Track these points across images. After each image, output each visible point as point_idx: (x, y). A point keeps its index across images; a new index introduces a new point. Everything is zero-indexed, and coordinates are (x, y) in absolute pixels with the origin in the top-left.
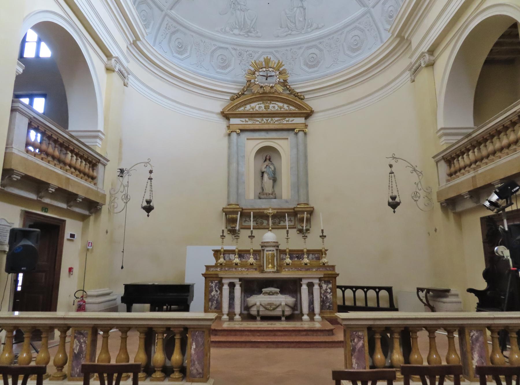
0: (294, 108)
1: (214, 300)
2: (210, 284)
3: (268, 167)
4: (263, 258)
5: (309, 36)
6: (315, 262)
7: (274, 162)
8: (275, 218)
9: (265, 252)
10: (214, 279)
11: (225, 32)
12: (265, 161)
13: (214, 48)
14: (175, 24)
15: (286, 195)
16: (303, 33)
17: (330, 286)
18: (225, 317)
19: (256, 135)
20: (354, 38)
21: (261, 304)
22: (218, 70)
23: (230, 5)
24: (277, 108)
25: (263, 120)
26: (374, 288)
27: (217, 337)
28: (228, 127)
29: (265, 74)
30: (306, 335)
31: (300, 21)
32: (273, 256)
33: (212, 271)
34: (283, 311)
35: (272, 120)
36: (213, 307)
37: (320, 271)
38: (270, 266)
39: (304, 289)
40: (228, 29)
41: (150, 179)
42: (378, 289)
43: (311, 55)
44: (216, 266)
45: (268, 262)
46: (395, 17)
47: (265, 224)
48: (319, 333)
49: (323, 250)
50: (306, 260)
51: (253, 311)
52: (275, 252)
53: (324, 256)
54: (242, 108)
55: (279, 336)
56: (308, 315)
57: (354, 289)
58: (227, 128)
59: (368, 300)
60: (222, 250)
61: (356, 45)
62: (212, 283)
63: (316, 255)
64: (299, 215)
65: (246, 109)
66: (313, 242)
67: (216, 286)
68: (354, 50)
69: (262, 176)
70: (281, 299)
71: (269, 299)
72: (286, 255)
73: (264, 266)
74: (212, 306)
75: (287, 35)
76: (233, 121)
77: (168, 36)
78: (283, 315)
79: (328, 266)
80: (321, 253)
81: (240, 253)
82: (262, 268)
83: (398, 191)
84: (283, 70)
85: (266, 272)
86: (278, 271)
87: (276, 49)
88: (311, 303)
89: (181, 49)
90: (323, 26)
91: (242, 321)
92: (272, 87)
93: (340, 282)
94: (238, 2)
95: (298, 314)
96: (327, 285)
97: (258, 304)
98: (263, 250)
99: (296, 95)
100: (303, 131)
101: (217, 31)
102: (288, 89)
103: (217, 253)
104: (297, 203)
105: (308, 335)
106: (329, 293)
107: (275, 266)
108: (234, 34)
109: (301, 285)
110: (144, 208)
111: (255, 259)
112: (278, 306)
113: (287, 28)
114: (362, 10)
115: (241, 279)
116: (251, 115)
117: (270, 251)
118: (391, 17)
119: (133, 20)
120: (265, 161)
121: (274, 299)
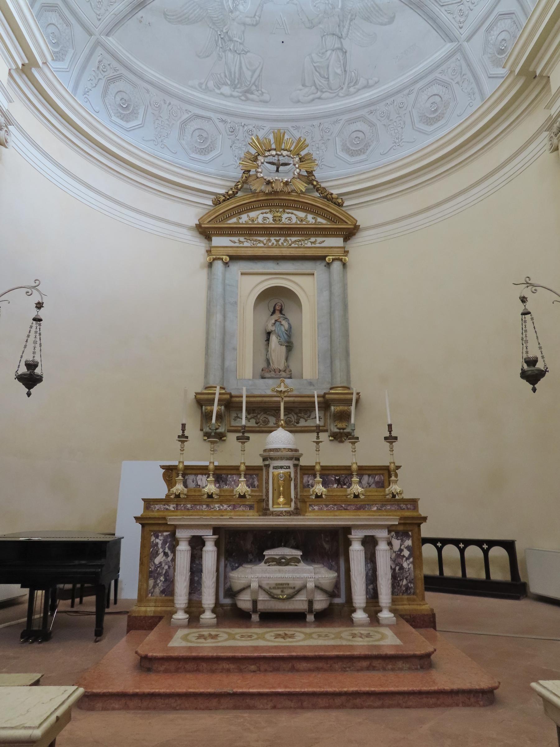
0: (324, 222)
1: (159, 574)
2: (153, 538)
3: (277, 323)
4: (267, 483)
5: (352, 100)
6: (375, 493)
7: (288, 316)
8: (289, 413)
9: (271, 470)
10: (162, 528)
11: (207, 90)
12: (274, 313)
13: (186, 116)
14: (115, 64)
15: (310, 373)
16: (341, 94)
17: (409, 542)
18: (181, 616)
19: (258, 267)
20: (431, 100)
21: (260, 587)
22: (194, 155)
23: (217, 42)
24: (294, 220)
25: (269, 240)
26: (479, 543)
27: (153, 676)
28: (209, 252)
29: (275, 160)
30: (368, 668)
31: (336, 73)
32: (288, 479)
33: (157, 511)
34: (311, 603)
35: (285, 240)
36: (157, 590)
37: (386, 511)
38: (281, 499)
39: (357, 550)
40: (211, 84)
41: (38, 320)
42: (486, 545)
43: (355, 135)
44: (166, 501)
45: (276, 492)
46: (509, 50)
47: (271, 424)
48: (400, 664)
49: (392, 467)
50: (356, 488)
51: (244, 602)
52: (292, 470)
53: (393, 478)
54: (234, 220)
55: (305, 671)
56: (365, 610)
57: (439, 544)
58: (206, 254)
59: (466, 563)
60: (181, 466)
61: (436, 110)
62: (157, 537)
63: (377, 478)
64: (332, 408)
65: (241, 221)
66: (368, 451)
67: (164, 543)
68: (430, 121)
69: (268, 340)
70: (306, 575)
71: (279, 575)
72: (315, 476)
73: (268, 501)
74: (154, 587)
75: (313, 100)
76: (217, 241)
77: (102, 83)
78: (311, 610)
79: (404, 501)
80: (386, 473)
81: (218, 472)
82: (264, 504)
83: (540, 348)
84: (307, 155)
85: (272, 514)
86: (297, 512)
87: (294, 124)
88: (372, 579)
89: (126, 110)
90: (376, 83)
91: (218, 625)
92: (287, 184)
93: (426, 531)
94: (229, 37)
95: (342, 605)
96: (403, 542)
97: (255, 585)
98: (268, 466)
99: (328, 197)
100: (341, 260)
101: (192, 87)
102: (315, 186)
103: (170, 473)
104: (329, 386)
105: (374, 668)
106: (407, 559)
107: (291, 500)
108: (222, 94)
109: (348, 543)
110: (21, 378)
111: (251, 485)
112: (298, 591)
113: (313, 88)
114: (449, 47)
115: (216, 530)
116: (251, 231)
117: (281, 467)
118: (501, 52)
119: (28, 33)
120: (274, 313)
121: (290, 575)
